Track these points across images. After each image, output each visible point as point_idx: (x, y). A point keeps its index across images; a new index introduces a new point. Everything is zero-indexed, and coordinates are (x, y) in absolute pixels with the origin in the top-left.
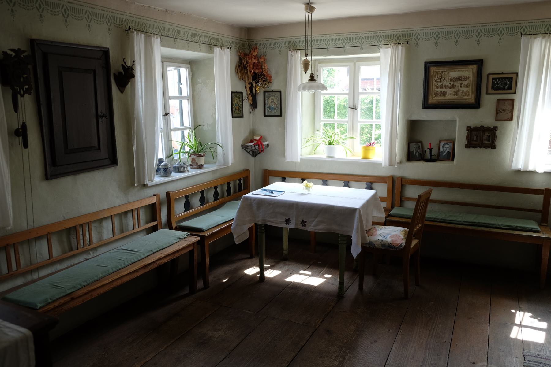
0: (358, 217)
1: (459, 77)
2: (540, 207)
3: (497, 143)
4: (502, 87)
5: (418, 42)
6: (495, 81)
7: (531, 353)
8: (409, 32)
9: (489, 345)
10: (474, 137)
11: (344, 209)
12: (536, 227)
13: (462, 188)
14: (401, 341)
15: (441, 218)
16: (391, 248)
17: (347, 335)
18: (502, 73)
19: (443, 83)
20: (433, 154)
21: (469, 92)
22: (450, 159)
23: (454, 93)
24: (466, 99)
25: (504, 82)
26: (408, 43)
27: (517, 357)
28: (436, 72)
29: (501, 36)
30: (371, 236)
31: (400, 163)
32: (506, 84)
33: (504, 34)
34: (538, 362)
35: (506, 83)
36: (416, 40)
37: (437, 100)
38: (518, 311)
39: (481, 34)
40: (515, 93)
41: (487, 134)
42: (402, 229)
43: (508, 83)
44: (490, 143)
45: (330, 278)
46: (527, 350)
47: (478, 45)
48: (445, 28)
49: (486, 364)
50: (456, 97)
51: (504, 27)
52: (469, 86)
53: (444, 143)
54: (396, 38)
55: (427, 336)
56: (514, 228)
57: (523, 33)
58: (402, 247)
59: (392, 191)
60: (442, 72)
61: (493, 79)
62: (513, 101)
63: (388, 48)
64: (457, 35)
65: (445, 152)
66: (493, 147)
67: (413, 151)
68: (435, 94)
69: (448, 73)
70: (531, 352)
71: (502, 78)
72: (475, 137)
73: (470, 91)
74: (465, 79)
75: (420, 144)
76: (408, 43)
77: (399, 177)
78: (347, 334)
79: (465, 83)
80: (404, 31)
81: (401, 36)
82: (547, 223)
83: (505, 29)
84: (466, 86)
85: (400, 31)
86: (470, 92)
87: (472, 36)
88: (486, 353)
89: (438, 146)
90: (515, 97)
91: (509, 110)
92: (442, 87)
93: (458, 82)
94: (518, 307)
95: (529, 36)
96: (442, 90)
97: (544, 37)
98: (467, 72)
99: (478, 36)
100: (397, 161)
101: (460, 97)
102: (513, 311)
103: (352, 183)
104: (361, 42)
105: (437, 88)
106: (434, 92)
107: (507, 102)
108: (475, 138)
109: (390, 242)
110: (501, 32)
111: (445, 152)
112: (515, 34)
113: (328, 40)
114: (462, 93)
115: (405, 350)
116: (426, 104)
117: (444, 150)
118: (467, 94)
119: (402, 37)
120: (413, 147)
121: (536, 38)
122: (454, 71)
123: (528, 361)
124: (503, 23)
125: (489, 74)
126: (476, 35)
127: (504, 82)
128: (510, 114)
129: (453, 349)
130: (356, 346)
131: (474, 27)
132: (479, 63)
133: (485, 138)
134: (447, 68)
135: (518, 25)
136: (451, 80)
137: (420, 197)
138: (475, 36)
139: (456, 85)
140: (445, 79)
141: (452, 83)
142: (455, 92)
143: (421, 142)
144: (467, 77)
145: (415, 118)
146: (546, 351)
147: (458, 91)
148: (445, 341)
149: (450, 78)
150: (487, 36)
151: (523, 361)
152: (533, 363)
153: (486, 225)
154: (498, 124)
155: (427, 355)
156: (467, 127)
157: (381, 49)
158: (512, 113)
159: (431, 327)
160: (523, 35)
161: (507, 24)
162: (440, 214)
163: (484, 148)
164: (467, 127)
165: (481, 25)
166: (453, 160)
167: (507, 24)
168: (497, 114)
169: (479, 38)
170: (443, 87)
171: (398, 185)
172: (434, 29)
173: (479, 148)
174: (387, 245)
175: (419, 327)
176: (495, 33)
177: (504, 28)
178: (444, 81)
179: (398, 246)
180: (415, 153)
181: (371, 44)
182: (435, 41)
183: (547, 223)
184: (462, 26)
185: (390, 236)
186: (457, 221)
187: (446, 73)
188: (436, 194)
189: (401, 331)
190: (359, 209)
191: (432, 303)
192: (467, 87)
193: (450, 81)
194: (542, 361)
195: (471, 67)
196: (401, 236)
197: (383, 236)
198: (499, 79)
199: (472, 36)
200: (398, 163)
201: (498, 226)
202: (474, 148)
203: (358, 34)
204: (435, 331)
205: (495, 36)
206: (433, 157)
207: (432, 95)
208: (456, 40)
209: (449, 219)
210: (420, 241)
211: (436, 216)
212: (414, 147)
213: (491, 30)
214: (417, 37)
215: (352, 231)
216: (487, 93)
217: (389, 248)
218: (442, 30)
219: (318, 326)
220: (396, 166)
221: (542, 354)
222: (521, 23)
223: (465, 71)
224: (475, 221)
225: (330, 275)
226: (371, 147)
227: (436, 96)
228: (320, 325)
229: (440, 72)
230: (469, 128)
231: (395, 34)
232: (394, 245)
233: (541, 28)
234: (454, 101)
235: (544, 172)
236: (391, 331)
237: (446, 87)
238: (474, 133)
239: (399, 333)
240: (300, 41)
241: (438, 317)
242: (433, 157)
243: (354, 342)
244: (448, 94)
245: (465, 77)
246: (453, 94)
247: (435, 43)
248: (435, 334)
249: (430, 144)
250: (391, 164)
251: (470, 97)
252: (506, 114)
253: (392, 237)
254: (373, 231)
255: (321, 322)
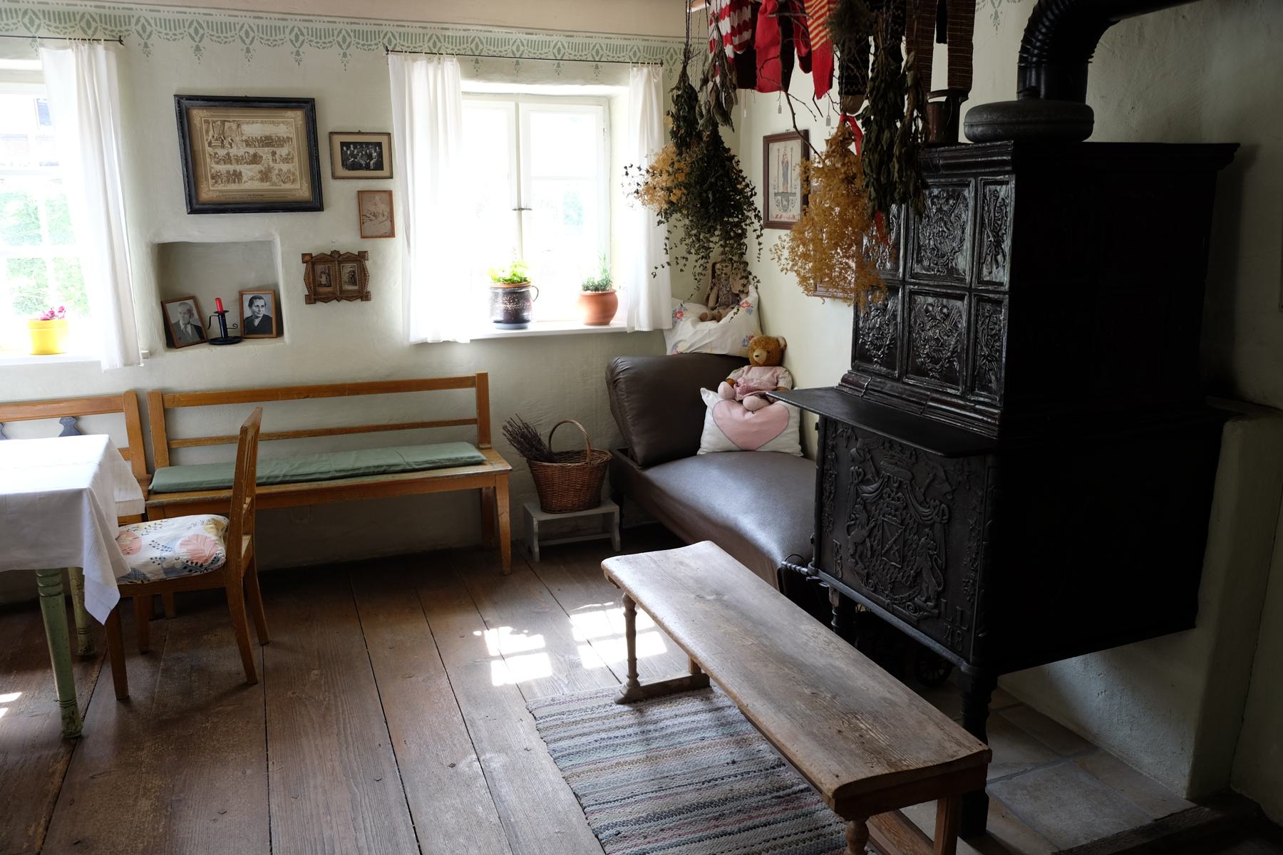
0: (91, 512)
1: (265, 137)
2: (472, 413)
3: (371, 287)
4: (363, 162)
5: (149, 42)
6: (347, 150)
7: (540, 701)
8: (117, 13)
9: (465, 717)
10: (321, 277)
11: (40, 499)
12: (474, 453)
13: (313, 397)
14: (284, 785)
15: (282, 473)
16: (190, 571)
17: (138, 829)
18: (359, 133)
19: (231, 151)
20: (229, 324)
21: (294, 174)
22: (271, 333)
23: (259, 176)
24: (291, 190)
25: (366, 153)
26: (120, 41)
27: (521, 720)
28: (207, 122)
29: (345, 48)
30: (128, 553)
31: (150, 354)
32: (370, 157)
33: (205, 37)
34: (558, 714)
35: (371, 154)
36: (140, 35)
37: (220, 191)
38: (484, 629)
39: (301, 38)
40: (391, 177)
41: (348, 268)
42: (205, 517)
43: (374, 154)
44: (356, 288)
45: (19, 701)
46: (531, 698)
47: (299, 64)
48: (214, 14)
49: (474, 756)
50: (266, 185)
51: (349, 28)
52: (292, 158)
53: (251, 296)
54: (83, 24)
55: (336, 750)
56: (439, 464)
57: (390, 48)
58: (220, 563)
59: (140, 430)
60: (223, 122)
61: (343, 144)
62: (390, 193)
63: (65, 48)
64: (247, 34)
65: (257, 317)
66: (364, 296)
67: (178, 323)
68: (213, 178)
69: (239, 126)
70: (539, 699)
71: (361, 144)
72: (324, 277)
73: (296, 170)
74: (281, 142)
75: (190, 302)
76: (120, 41)
77: (153, 393)
78: (137, 827)
79: (283, 151)
80: (104, 7)
81: (485, 43)
82: (489, 442)
83: (352, 34)
84: (287, 160)
85: (91, 6)
86: (298, 173)
87: (282, 42)
88: (466, 734)
89: (238, 303)
90: (394, 185)
91: (386, 214)
92: (228, 159)
93: (266, 149)
94: (483, 623)
95: (402, 55)
96: (231, 168)
97: (430, 61)
98: (282, 125)
99: (294, 42)
100: (143, 352)
101: (276, 185)
102: (477, 633)
103: (87, 421)
104: (671, 59)
105: (217, 163)
106: (211, 171)
107: (377, 197)
108: (324, 280)
109: (185, 557)
110: (344, 39)
111: (257, 317)
112: (372, 48)
113: (34, 13)
114: (279, 175)
115: (304, 802)
116: (194, 201)
117: (253, 312)
118: (288, 178)
119: (485, 45)
120: (177, 313)
121: (414, 60)
122: (253, 123)
123: (541, 718)
124: (346, 20)
125: (331, 134)
126: (291, 41)
127: (366, 153)
128: (388, 223)
129: (402, 755)
130: (177, 845)
131: (283, 19)
132: (307, 106)
133: (345, 277)
134: (235, 114)
135: (422, 31)
136: (248, 143)
137: (244, 431)
138: (289, 42)
139: (262, 157)
140: (232, 140)
141: (252, 151)
142: (261, 172)
143: (193, 298)
144: (285, 137)
145: (169, 237)
146: (562, 689)
147: (269, 170)
148: (380, 745)
149: (244, 138)
150: (316, 45)
151: (534, 723)
152: (551, 719)
153: (383, 469)
154: (366, 245)
155: (356, 790)
156: (304, 255)
157: (42, 50)
158: (391, 221)
159: (335, 727)
160: (390, 52)
161: (354, 23)
162: (277, 464)
163: (345, 301)
164: (302, 254)
165: (298, 17)
166: (280, 333)
167: (354, 23)
168: (362, 223)
169: (299, 48)
170: (231, 160)
171: (153, 414)
172: (185, 13)
173: (335, 302)
174: (178, 566)
175: (311, 737)
176: (331, 39)
177: (350, 31)
178: (231, 145)
179: (210, 562)
180: (182, 327)
181: (7, 30)
182: (194, 44)
183: (489, 442)
184: (256, 14)
185: (180, 541)
186: (321, 473)
187: (234, 126)
188: (274, 418)
189: (273, 763)
190: (90, 491)
191: (316, 672)
192: (288, 163)
193: (245, 146)
194: (563, 708)
195: (290, 113)
196: (209, 535)
197: (160, 546)
198: (355, 144)
199: (282, 42)
200: (146, 357)
201: (408, 467)
202: (326, 302)
203: (335, 22)
204: (349, 731)
205: (333, 46)
206: (231, 333)
207: (207, 180)
208: (245, 47)
209: (301, 471)
210: (252, 537)
211: (268, 471)
212: (180, 310)
213: (580, 46)
214: (144, 28)
215: (79, 550)
216: (334, 177)
217: (186, 573)
218: (209, 18)
219: (40, 843)
220: (142, 365)
221: (557, 695)
222: (382, 25)
223: (279, 123)
224: (358, 465)
225: (14, 691)
226: (54, 321)
227: (216, 182)
228: (45, 836)
229: (219, 123)
230: (307, 258)
231: (238, 23)
232: (197, 563)
233: (421, 40)
234: (262, 195)
235: (472, 341)
236: (249, 772)
237: (239, 160)
238: (320, 268)
239: (270, 769)
240: (449, 36)
241: (341, 700)
242: (231, 333)
243: (168, 838)
244: (245, 178)
245: (279, 138)
246: (258, 177)
247: (194, 48)
248: (352, 738)
249: (219, 300)
250: (128, 362)
251: (297, 186)
252: (380, 223)
253: (187, 545)
254: (127, 541)
255: (47, 829)
